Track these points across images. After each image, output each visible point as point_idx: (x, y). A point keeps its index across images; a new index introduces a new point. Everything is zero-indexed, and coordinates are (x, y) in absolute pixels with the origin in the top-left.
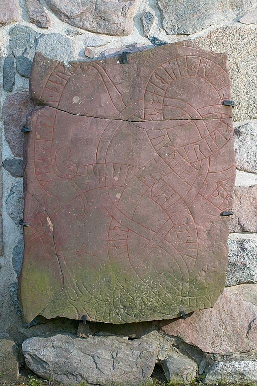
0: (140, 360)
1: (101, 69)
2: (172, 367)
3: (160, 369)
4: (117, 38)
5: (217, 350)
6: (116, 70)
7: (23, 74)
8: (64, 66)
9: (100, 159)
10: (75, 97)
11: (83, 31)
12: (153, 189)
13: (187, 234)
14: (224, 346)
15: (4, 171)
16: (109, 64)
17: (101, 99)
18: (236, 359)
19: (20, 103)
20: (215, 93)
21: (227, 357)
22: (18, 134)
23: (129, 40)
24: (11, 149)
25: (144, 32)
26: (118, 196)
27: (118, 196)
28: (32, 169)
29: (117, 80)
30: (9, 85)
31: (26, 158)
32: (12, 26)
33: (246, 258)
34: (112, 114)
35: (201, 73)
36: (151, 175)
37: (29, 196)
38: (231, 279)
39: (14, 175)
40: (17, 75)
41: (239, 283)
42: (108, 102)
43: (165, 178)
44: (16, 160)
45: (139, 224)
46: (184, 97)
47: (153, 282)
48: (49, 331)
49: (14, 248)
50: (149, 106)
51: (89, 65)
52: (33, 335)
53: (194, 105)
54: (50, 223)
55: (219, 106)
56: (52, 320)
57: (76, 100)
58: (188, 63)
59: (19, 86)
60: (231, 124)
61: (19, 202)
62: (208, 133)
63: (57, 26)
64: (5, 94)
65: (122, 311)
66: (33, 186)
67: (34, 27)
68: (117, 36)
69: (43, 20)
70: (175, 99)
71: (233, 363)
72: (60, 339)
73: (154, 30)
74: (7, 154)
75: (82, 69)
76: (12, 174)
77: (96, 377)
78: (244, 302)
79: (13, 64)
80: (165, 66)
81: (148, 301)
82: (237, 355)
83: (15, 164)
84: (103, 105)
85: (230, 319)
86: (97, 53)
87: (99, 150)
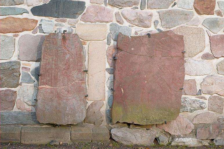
0: (150, 137)
2: (161, 139)
3: (156, 140)
4: (146, 28)
5: (175, 134)
6: (146, 40)
8: (129, 38)
11: (134, 25)
14: (178, 133)
15: (106, 72)
18: (182, 138)
21: (179, 137)
23: (149, 29)
25: (155, 26)
26: (146, 82)
27: (146, 82)
28: (117, 72)
29: (147, 43)
30: (108, 43)
31: (114, 68)
32: (111, 23)
33: (186, 104)
35: (177, 42)
37: (116, 81)
38: (181, 110)
41: (183, 112)
42: (143, 50)
43: (162, 76)
50: (157, 52)
51: (137, 39)
52: (115, 128)
53: (172, 52)
54: (123, 90)
57: (133, 49)
58: (171, 38)
63: (126, 24)
64: (107, 46)
66: (117, 78)
67: (118, 24)
68: (146, 27)
69: (121, 21)
71: (181, 139)
72: (125, 129)
73: (159, 27)
74: (108, 66)
75: (135, 39)
76: (109, 73)
77: (135, 142)
80: (163, 39)
81: (154, 116)
82: (182, 136)
86: (139, 34)
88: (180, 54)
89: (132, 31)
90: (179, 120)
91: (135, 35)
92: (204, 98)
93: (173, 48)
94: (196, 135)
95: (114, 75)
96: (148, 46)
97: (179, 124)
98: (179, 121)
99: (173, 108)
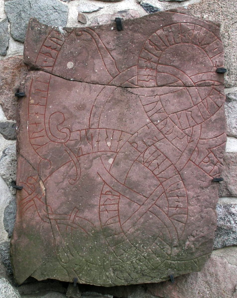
1: (95, 36)
6: (108, 39)
7: (17, 39)
8: (58, 32)
9: (92, 124)
10: (69, 63)
12: (145, 155)
13: (178, 200)
16: (103, 30)
17: (94, 64)
19: (13, 67)
20: (209, 60)
22: (11, 98)
24: (4, 111)
29: (111, 46)
34: (105, 79)
35: (202, 44)
36: (143, 141)
39: (6, 138)
40: (11, 39)
44: (9, 123)
45: (131, 189)
46: (177, 64)
47: (143, 246)
48: (39, 290)
49: (6, 209)
53: (188, 72)
55: (212, 73)
56: (43, 281)
57: (70, 65)
58: (182, 30)
59: (13, 50)
60: (223, 92)
61: (11, 164)
62: (201, 100)
65: (112, 274)
70: (168, 65)
75: (77, 35)
78: (229, 265)
79: (7, 29)
80: (159, 32)
83: (8, 126)
84: (96, 71)
85: (216, 281)
87: (91, 116)
88: (209, 76)
89: (70, 11)
90: (212, 270)
91: (79, 26)
92: (50, 53)
93: (189, 60)
94: (160, 37)
95: (17, 142)
96: (114, 54)
97: (213, 281)
98: (211, 275)
99: (194, 236)
